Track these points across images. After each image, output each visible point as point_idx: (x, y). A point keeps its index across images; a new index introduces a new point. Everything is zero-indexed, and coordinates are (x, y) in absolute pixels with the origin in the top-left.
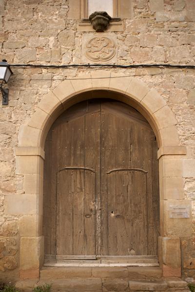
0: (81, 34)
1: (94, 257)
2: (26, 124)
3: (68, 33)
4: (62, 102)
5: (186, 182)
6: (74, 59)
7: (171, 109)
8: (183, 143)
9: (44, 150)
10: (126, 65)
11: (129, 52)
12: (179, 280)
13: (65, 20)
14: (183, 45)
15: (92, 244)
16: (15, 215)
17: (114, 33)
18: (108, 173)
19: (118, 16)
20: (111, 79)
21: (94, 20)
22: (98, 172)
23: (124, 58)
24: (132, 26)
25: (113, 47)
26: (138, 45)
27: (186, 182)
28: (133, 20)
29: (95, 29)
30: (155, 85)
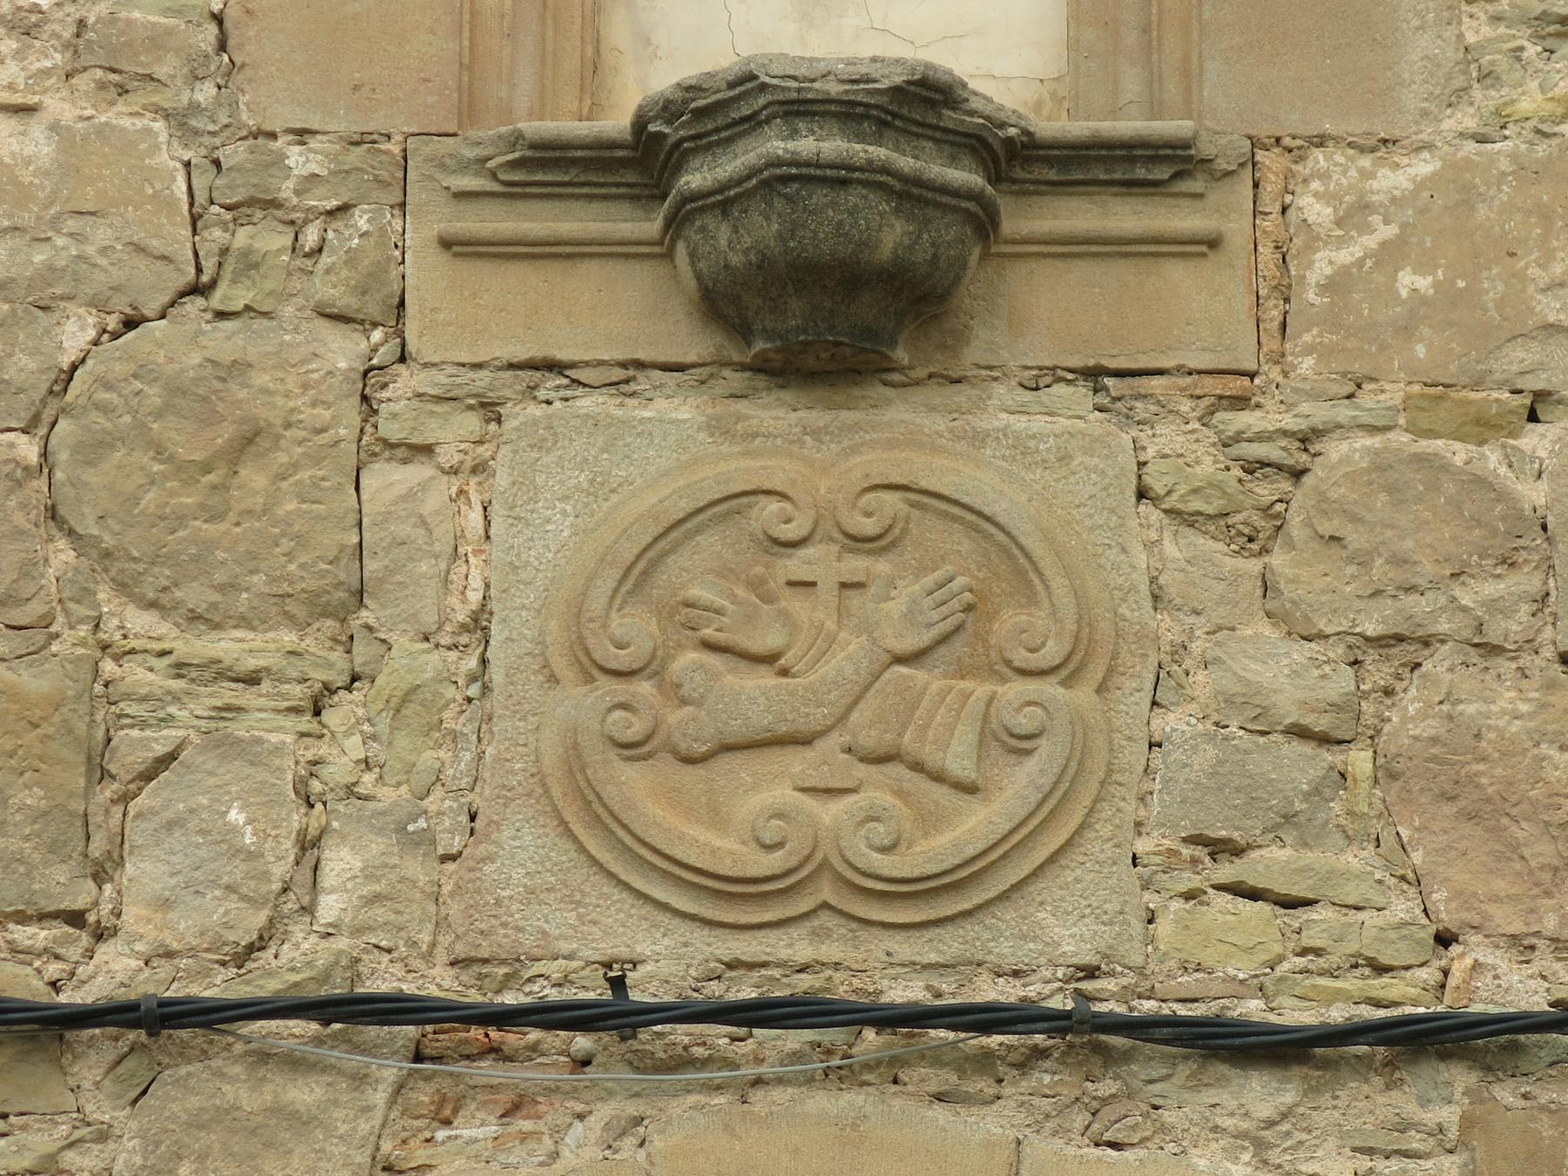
0: (490, 409)
3: (237, 368)
6: (339, 862)
10: (1297, 1015)
11: (1360, 760)
13: (181, 121)
17: (1079, 395)
21: (724, 201)
23: (1256, 868)
24: (1409, 281)
25: (1066, 670)
26: (1511, 627)
28: (1424, 166)
29: (742, 330)
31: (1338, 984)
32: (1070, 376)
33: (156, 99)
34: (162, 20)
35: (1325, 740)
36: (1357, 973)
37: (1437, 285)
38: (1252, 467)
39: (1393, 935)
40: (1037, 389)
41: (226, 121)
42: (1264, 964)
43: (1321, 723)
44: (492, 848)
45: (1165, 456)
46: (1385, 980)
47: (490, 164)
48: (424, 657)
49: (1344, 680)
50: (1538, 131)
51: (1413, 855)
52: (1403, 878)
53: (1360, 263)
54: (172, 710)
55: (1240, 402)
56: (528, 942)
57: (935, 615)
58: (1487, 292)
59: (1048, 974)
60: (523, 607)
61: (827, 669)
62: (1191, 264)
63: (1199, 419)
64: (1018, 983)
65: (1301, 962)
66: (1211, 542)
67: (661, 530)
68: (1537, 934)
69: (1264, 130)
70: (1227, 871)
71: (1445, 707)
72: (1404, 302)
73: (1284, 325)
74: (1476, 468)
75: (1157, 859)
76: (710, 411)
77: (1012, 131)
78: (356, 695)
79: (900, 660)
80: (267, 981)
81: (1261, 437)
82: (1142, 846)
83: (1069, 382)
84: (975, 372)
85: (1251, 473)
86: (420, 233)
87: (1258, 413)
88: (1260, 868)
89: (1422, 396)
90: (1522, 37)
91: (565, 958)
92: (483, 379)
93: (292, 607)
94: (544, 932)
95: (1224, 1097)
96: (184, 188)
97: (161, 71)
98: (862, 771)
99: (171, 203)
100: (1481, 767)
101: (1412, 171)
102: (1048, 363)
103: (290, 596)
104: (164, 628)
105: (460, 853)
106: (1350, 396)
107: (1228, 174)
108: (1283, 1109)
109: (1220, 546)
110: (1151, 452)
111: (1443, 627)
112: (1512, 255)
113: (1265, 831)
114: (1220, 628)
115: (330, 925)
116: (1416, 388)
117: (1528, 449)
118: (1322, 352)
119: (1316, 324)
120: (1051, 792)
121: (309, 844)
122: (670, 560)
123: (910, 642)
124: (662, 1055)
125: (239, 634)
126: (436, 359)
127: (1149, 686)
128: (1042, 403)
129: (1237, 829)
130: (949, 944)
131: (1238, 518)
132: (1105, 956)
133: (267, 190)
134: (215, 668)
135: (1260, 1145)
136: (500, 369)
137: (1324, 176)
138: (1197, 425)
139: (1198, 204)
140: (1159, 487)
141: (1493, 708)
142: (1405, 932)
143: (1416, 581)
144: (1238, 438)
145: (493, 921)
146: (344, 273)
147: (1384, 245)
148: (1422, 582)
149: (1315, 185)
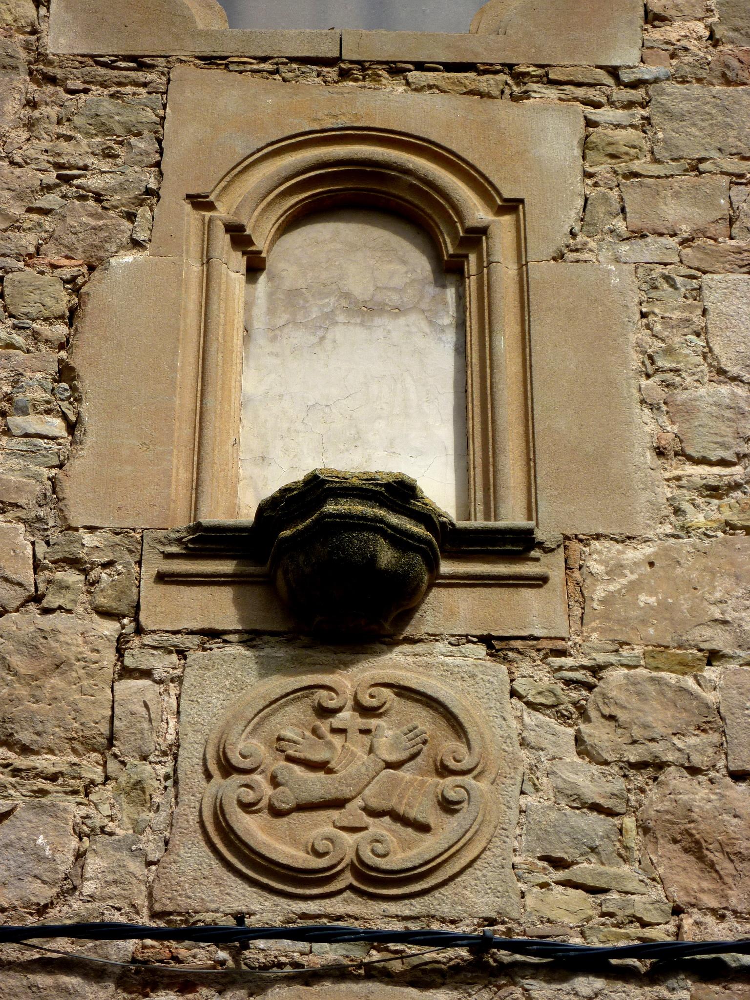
0: (182, 653)
6: (93, 864)
24: (643, 598)
31: (622, 931)
32: (475, 640)
33: (19, 514)
34: (24, 480)
35: (610, 813)
36: (633, 925)
37: (658, 601)
38: (568, 682)
39: (650, 907)
40: (458, 645)
41: (53, 524)
42: (582, 920)
43: (606, 803)
44: (176, 858)
45: (524, 677)
46: (646, 929)
47: (184, 540)
48: (144, 767)
49: (621, 784)
50: (705, 534)
51: (659, 868)
52: (654, 880)
53: (619, 591)
54: (11, 792)
55: (562, 653)
56: (196, 905)
57: (409, 744)
58: (683, 605)
59: (468, 922)
60: (195, 742)
62: (534, 590)
63: (541, 660)
64: (453, 926)
65: (603, 920)
66: (548, 719)
67: (267, 703)
68: (726, 908)
69: (569, 532)
70: (561, 875)
71: (671, 796)
72: (642, 608)
73: (582, 618)
74: (682, 684)
75: (526, 867)
76: (292, 653)
77: (445, 519)
78: (108, 787)
81: (571, 669)
83: (474, 643)
84: (427, 637)
85: (568, 686)
86: (148, 573)
87: (570, 658)
88: (578, 872)
89: (653, 651)
90: (695, 495)
91: (213, 912)
92: (177, 639)
93: (77, 745)
94: (202, 899)
96: (31, 553)
97: (22, 501)
98: (369, 820)
99: (24, 559)
100: (692, 825)
101: (644, 551)
102: (464, 633)
103: (75, 739)
105: (159, 861)
106: (616, 651)
107: (552, 550)
108: (597, 991)
109: (553, 720)
110: (516, 675)
112: (695, 589)
113: (582, 855)
114: (554, 758)
115: (89, 896)
116: (650, 648)
117: (708, 677)
118: (602, 631)
120: (468, 830)
122: (272, 719)
123: (394, 757)
124: (264, 961)
125: (49, 756)
126: (154, 628)
127: (519, 783)
128: (461, 652)
129: (567, 853)
130: (415, 907)
131: (562, 707)
132: (499, 913)
133: (73, 554)
134: (35, 771)
136: (187, 634)
137: (599, 553)
138: (539, 663)
139: (537, 564)
140: (521, 691)
141: (697, 797)
142: (656, 906)
143: (654, 736)
144: (561, 668)
145: (175, 893)
146: (110, 592)
147: (631, 583)
148: (658, 737)
149: (595, 556)
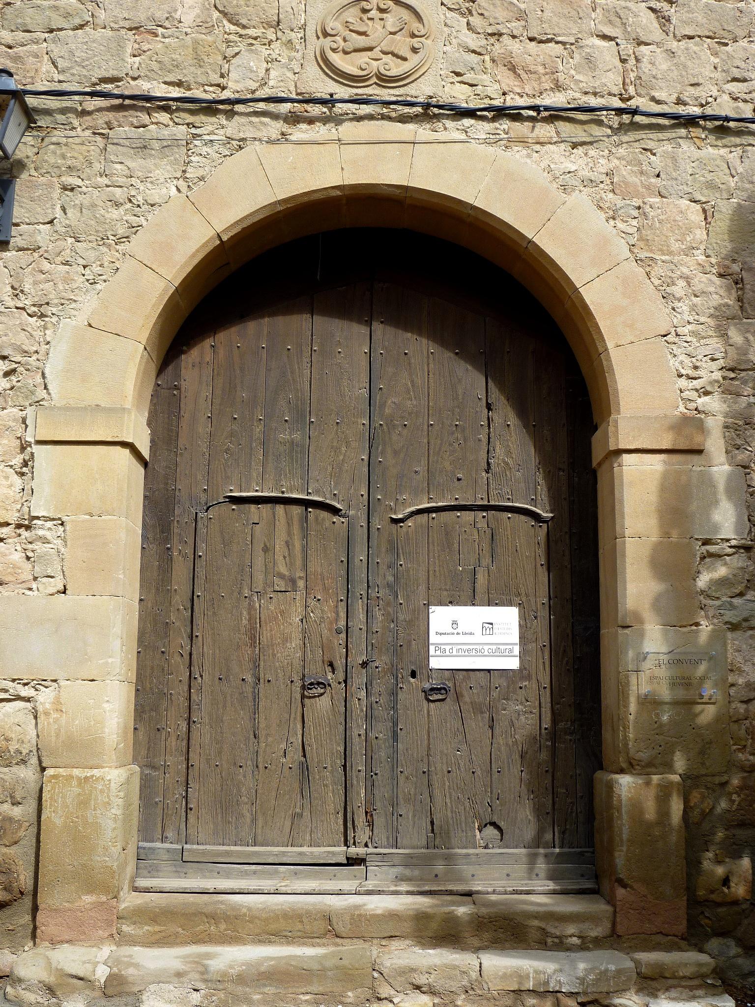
1: (339, 852)
2: (81, 320)
4: (225, 238)
5: (703, 558)
6: (273, 73)
7: (648, 274)
8: (692, 405)
9: (149, 424)
12: (680, 949)
14: (691, 38)
15: (332, 799)
16: (26, 678)
18: (396, 521)
19: (489, 502)
20: (411, 139)
22: (358, 514)
27: (703, 558)
30: (590, 182)
35: (480, 54)
43: (478, 50)
49: (484, 42)
61: (376, 35)
70: (459, 79)
79: (391, 33)
80: (258, 95)
82: (442, 73)
93: (265, 25)
95: (460, 123)
98: (383, 56)
104: (238, 29)
111: (504, 31)
119: (708, 814)
121: (267, 70)
123: (393, 30)
135: (466, 132)
